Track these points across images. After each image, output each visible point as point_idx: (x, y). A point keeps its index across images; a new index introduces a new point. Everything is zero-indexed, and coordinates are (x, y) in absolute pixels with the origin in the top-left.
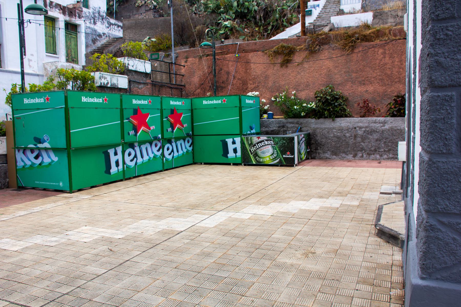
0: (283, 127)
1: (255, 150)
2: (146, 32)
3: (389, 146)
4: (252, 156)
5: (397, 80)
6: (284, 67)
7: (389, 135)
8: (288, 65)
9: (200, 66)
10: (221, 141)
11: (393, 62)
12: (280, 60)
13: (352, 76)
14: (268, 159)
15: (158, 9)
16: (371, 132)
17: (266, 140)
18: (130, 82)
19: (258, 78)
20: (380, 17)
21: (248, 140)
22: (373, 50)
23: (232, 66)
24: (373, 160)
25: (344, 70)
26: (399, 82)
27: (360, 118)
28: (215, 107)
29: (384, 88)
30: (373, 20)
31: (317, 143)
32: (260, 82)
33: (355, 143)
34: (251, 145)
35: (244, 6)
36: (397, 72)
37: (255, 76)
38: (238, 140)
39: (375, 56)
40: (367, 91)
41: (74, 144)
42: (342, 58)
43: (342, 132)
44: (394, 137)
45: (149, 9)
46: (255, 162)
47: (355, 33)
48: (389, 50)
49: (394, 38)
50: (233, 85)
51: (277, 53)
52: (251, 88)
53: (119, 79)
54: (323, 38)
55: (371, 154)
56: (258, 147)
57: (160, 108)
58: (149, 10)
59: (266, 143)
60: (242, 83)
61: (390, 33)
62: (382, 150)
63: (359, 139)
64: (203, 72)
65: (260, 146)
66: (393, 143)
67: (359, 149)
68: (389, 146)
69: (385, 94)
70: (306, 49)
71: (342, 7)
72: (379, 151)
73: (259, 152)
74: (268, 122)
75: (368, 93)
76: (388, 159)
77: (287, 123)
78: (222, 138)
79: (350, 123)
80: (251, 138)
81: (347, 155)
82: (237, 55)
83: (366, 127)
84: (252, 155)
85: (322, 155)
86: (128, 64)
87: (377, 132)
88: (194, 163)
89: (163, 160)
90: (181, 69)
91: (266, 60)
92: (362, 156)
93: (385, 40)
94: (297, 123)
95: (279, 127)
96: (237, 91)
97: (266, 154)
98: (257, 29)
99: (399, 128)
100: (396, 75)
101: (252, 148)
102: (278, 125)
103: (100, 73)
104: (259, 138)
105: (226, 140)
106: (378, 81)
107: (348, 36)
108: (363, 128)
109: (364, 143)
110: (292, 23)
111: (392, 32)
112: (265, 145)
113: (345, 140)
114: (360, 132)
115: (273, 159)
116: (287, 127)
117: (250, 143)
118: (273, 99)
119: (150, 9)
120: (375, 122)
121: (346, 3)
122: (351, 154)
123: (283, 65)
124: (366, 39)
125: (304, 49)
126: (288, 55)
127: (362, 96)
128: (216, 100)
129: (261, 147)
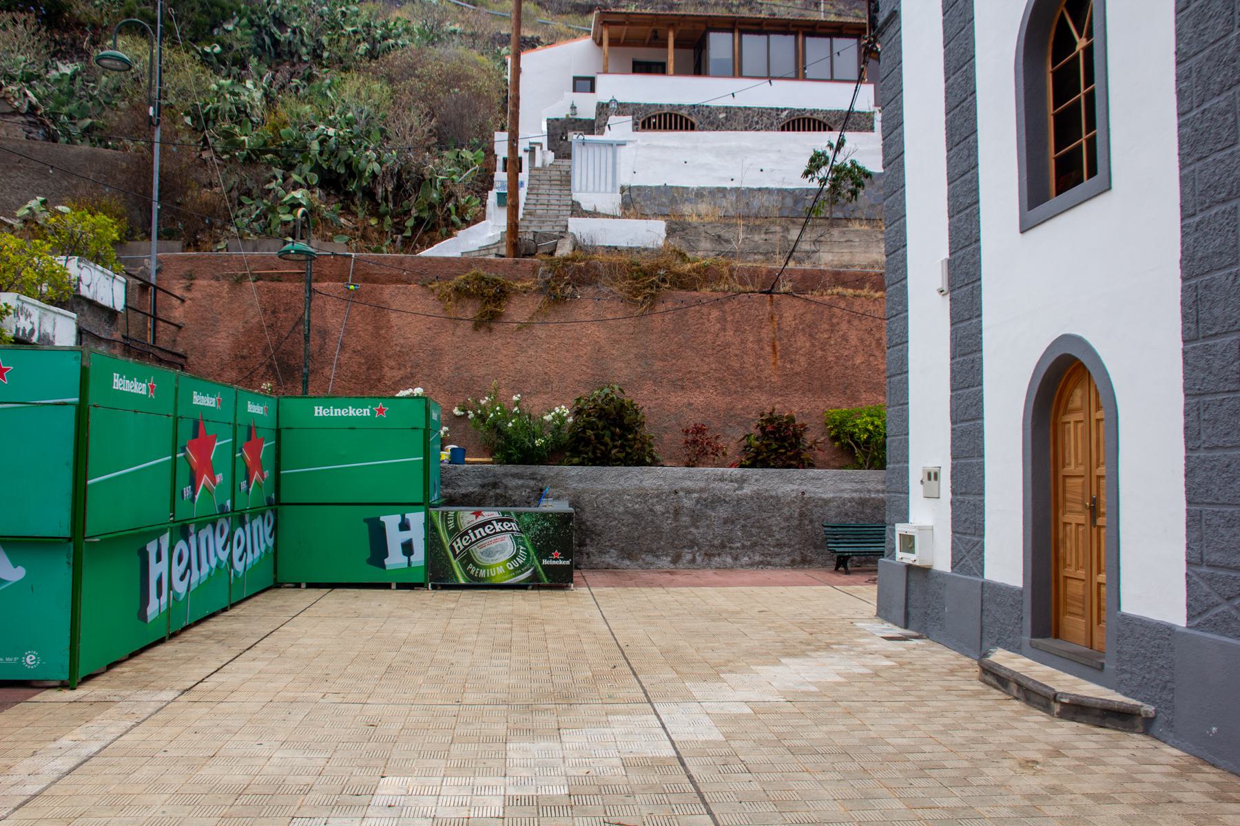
0: (495, 485)
1: (466, 547)
2: (26, 180)
3: (752, 535)
4: (455, 563)
5: (753, 383)
6: (482, 331)
7: (753, 510)
8: (493, 325)
9: (235, 306)
10: (366, 520)
11: (742, 342)
12: (471, 310)
13: (655, 368)
14: (500, 570)
15: (41, 115)
16: (712, 502)
17: (498, 521)
18: (80, 332)
19: (411, 353)
20: (682, 233)
21: (447, 520)
22: (699, 311)
23: (335, 313)
24: (718, 568)
25: (634, 351)
26: (760, 387)
27: (687, 469)
28: (352, 426)
29: (728, 399)
30: (667, 238)
31: (583, 527)
32: (418, 365)
33: (676, 529)
34: (455, 532)
35: (336, 156)
36: (753, 365)
37: (402, 347)
38: (417, 519)
39: (703, 324)
40: (690, 404)
41: (95, 525)
42: (627, 321)
43: (646, 502)
44: (765, 515)
45: (9, 110)
46: (464, 578)
47: (658, 267)
48: (733, 315)
49: (741, 288)
50: (339, 366)
51: (461, 293)
52: (393, 380)
53: (59, 319)
54: (579, 269)
55: (714, 555)
56: (474, 539)
57: (232, 422)
58: (9, 114)
59: (498, 527)
60: (366, 363)
61: (731, 275)
62: (739, 545)
63: (685, 519)
64: (246, 323)
65: (479, 536)
66: (761, 527)
67: (685, 542)
68: (752, 535)
69: (732, 413)
70: (540, 291)
71: (576, 197)
72: (731, 548)
73: (477, 551)
74: (454, 472)
75: (693, 410)
76: (752, 565)
77: (506, 475)
78: (370, 512)
79: (664, 479)
80: (456, 513)
81: (658, 557)
82: (352, 287)
83: (702, 490)
84: (458, 559)
85: (596, 559)
86: (79, 279)
87: (725, 502)
88: (277, 585)
89: (230, 574)
90: (171, 307)
91: (431, 308)
92: (693, 560)
93: (723, 291)
94: (532, 477)
95: (483, 486)
96: (352, 385)
97: (497, 556)
98: (373, 222)
99: (774, 493)
100: (752, 372)
101: (458, 540)
102: (479, 481)
103: (18, 299)
104: (478, 514)
105: (382, 518)
106: (713, 382)
107: (641, 270)
108: (694, 491)
109: (697, 528)
110: (468, 218)
111: (735, 273)
112: (496, 533)
113: (652, 521)
114: (688, 503)
115: (516, 569)
116: (506, 487)
117: (451, 526)
118: (456, 411)
119: (16, 112)
120: (722, 480)
121: (584, 189)
122: (667, 555)
123: (480, 327)
124: (681, 282)
125: (535, 291)
126: (494, 301)
127: (681, 416)
128: (355, 407)
129: (483, 537)
